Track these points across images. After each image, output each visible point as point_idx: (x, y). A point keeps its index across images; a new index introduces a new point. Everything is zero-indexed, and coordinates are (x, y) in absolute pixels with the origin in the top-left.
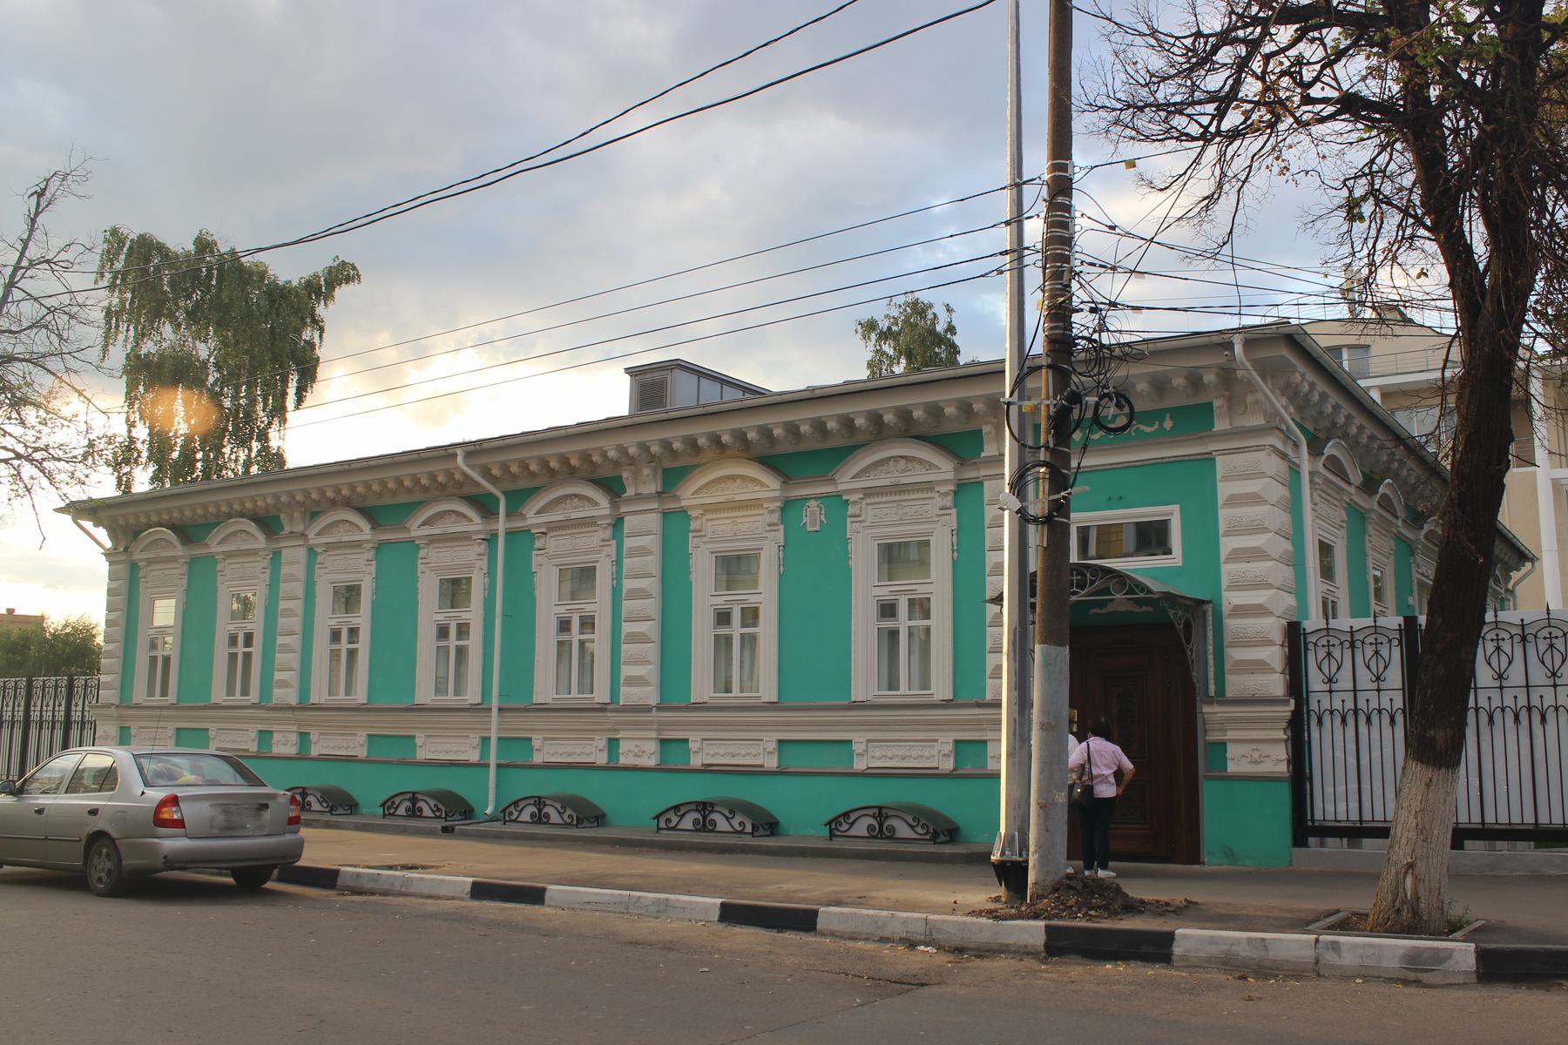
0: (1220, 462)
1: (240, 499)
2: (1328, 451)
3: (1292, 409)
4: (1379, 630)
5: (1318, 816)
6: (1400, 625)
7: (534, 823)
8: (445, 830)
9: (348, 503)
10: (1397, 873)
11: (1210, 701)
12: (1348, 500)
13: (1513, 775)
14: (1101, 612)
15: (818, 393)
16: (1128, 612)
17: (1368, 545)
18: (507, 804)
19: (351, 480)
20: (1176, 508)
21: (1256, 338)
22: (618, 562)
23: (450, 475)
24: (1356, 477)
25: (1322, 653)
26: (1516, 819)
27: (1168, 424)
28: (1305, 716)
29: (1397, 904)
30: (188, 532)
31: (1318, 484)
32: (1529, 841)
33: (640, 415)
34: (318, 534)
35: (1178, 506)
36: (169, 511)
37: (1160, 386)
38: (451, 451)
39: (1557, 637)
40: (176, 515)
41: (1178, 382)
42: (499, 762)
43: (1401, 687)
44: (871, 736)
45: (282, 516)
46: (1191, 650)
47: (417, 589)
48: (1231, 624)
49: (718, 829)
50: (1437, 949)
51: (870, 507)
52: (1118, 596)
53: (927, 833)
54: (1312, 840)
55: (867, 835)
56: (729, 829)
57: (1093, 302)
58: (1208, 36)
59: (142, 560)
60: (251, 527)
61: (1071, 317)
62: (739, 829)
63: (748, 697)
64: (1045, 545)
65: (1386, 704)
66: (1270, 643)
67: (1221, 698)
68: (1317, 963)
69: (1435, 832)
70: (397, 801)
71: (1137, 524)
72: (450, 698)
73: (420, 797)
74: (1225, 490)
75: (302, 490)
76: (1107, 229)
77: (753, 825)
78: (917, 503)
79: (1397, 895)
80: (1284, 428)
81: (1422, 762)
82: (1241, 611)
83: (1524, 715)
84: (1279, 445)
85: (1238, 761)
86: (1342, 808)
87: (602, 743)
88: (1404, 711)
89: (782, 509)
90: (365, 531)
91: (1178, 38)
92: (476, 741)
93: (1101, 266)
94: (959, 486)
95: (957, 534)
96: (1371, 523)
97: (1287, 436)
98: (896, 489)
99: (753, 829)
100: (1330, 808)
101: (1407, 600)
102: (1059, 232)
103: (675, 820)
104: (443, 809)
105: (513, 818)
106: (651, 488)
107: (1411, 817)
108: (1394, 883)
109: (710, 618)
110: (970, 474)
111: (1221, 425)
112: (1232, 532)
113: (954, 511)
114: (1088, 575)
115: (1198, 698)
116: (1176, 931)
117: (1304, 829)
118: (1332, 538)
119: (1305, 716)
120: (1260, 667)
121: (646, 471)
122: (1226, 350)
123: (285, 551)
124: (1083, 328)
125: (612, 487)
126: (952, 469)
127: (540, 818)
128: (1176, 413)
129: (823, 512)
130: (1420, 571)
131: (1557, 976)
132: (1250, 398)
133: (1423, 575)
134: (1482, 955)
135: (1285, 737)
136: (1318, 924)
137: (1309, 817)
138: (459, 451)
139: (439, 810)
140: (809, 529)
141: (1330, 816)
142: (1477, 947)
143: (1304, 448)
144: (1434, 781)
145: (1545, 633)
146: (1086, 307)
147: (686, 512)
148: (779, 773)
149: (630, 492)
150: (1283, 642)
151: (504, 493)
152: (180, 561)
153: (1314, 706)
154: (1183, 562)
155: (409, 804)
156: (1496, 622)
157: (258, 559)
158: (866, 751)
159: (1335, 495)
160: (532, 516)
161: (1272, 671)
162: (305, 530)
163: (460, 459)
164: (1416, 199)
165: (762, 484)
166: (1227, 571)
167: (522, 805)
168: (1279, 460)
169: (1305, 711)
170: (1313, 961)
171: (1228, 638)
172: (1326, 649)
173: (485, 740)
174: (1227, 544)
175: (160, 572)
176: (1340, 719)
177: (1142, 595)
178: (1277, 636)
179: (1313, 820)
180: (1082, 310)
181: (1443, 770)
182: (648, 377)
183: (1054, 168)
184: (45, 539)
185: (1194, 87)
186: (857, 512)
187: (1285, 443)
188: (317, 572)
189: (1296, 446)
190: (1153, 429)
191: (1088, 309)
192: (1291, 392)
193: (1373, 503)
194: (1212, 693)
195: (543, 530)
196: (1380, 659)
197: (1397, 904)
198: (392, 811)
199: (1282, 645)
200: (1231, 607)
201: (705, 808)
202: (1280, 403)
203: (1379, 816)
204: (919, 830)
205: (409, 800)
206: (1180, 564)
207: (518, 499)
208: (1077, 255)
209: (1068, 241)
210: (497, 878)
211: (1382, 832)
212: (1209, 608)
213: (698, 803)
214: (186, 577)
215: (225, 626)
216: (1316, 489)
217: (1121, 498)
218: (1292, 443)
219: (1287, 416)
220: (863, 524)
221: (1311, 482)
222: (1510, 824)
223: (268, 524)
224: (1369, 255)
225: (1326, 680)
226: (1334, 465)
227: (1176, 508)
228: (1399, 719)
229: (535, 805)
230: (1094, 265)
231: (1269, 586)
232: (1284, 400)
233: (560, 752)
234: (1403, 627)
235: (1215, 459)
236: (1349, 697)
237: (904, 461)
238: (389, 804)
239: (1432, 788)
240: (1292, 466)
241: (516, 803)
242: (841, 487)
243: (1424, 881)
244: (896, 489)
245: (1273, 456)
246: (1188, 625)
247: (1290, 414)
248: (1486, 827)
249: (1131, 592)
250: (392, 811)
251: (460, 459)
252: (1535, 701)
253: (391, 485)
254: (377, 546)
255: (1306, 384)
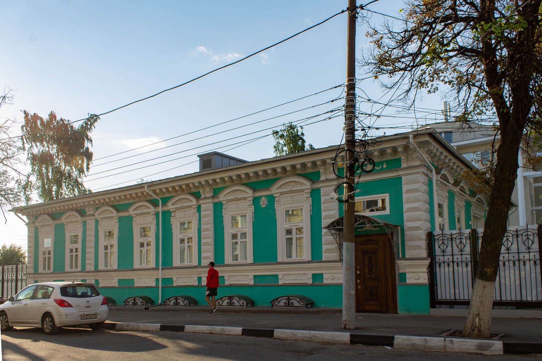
0: (404, 179)
1: (63, 206)
2: (442, 172)
3: (430, 159)
4: (444, 235)
5: (439, 297)
6: (470, 232)
7: (133, 305)
8: (146, 309)
9: (108, 204)
10: (473, 317)
11: (400, 259)
12: (449, 189)
13: (466, 285)
14: (361, 230)
15: (265, 161)
16: (370, 230)
17: (455, 204)
18: (166, 299)
19: (114, 195)
20: (387, 195)
21: (417, 134)
22: (200, 220)
23: (142, 193)
24: (452, 181)
25: (440, 242)
26: (448, 298)
27: (385, 166)
28: (434, 264)
29: (473, 328)
30: (53, 216)
31: (438, 184)
32: (447, 305)
33: (203, 172)
34: (98, 215)
35: (388, 194)
36: (47, 209)
37: (382, 152)
38: (143, 185)
39: (530, 235)
40: (50, 210)
41: (309, 165)
42: (163, 286)
43: (470, 253)
44: (284, 273)
45: (86, 209)
46: (393, 242)
47: (133, 231)
48: (407, 233)
49: (294, 305)
50: (489, 343)
51: (282, 198)
52: (368, 225)
53: (304, 304)
54: (437, 306)
55: (284, 305)
56: (239, 305)
57: (363, 127)
58: (410, 31)
59: (39, 226)
60: (76, 214)
61: (354, 132)
62: (242, 305)
63: (244, 262)
64: (346, 210)
65: (464, 259)
66: (421, 239)
67: (404, 258)
68: (445, 347)
69: (487, 303)
70: (129, 300)
71: (367, 201)
72: (74, 269)
73: (137, 298)
74: (405, 188)
75: (172, 186)
76: (367, 101)
77: (247, 303)
78: (288, 197)
79: (473, 325)
80: (427, 165)
81: (482, 280)
82: (411, 229)
83: (451, 264)
84: (425, 171)
85: (411, 280)
86: (448, 294)
87: (196, 279)
88: (471, 262)
89: (253, 200)
90: (115, 213)
91: (398, 33)
92: (154, 279)
93: (365, 114)
94: (312, 190)
95: (254, 214)
96: (457, 196)
97: (428, 168)
98: (291, 192)
99: (247, 305)
100: (444, 294)
101: (469, 223)
102: (351, 103)
103: (221, 302)
104: (145, 302)
105: (168, 304)
106: (210, 195)
107: (478, 299)
108: (472, 321)
109: (230, 237)
110: (316, 186)
111: (404, 165)
112: (408, 202)
113: (311, 199)
114: (358, 218)
115: (396, 258)
116: (395, 336)
117: (434, 302)
118: (442, 202)
119: (434, 264)
120: (418, 247)
121: (208, 189)
122: (406, 139)
123: (202, 206)
124: (359, 136)
125: (197, 196)
126: (310, 185)
127: (177, 304)
128: (387, 162)
129: (267, 200)
130: (474, 212)
131: (532, 353)
132: (414, 156)
133: (475, 213)
134: (505, 345)
135: (427, 271)
136: (444, 334)
137: (436, 298)
138: (145, 186)
139: (143, 302)
140: (262, 206)
141: (457, 298)
142: (503, 342)
143: (434, 172)
144: (487, 286)
145: (525, 234)
146: (360, 129)
147: (221, 202)
148: (312, 285)
149: (203, 196)
150: (426, 239)
151: (161, 199)
152: (248, 199)
153: (437, 260)
154: (390, 213)
155: (133, 301)
156: (442, 234)
157: (246, 201)
158: (283, 278)
159: (444, 187)
160: (170, 206)
161: (422, 249)
162: (94, 213)
163: (146, 188)
164: (485, 83)
165: (246, 192)
166: (406, 215)
167: (170, 299)
168: (425, 177)
169: (434, 262)
170: (444, 346)
171: (406, 238)
172: (459, 240)
173: (157, 280)
174: (406, 206)
175: (45, 229)
176: (456, 265)
177: (376, 225)
178: (424, 237)
179: (437, 299)
180: (358, 130)
181: (490, 282)
182: (205, 158)
183: (349, 81)
184: (7, 220)
185: (404, 51)
186: (226, 207)
187: (427, 170)
188: (99, 227)
189: (431, 171)
190: (379, 168)
191: (361, 129)
192: (429, 152)
193: (456, 189)
194: (401, 257)
195: (174, 210)
196: (444, 245)
197: (473, 328)
198: (127, 304)
199: (426, 240)
200: (407, 227)
201: (231, 298)
202: (425, 156)
203: (466, 298)
204: (301, 303)
205: (133, 300)
206: (389, 213)
207: (165, 201)
208: (357, 111)
209: (354, 106)
210: (168, 324)
211: (466, 303)
212: (399, 228)
213: (228, 297)
214: (54, 231)
215: (68, 246)
216: (438, 186)
217: (368, 192)
218: (429, 170)
219: (428, 161)
220: (280, 204)
221: (436, 183)
222: (511, 300)
223: (81, 212)
224: (465, 105)
225: (442, 252)
226: (444, 177)
227: (387, 195)
228: (469, 264)
229: (175, 299)
230: (362, 114)
231: (421, 220)
232: (427, 156)
233: (235, 280)
234: (471, 233)
235: (401, 177)
236: (450, 257)
237: (294, 183)
238: (127, 301)
239: (486, 288)
240: (429, 178)
241: (168, 299)
242: (273, 192)
243: (483, 320)
244: (291, 192)
245: (423, 175)
246: (392, 234)
247: (429, 160)
248: (456, 301)
249: (373, 223)
250: (127, 304)
251: (146, 188)
252: (455, 259)
253: (117, 198)
254: (156, 213)
255: (435, 150)
